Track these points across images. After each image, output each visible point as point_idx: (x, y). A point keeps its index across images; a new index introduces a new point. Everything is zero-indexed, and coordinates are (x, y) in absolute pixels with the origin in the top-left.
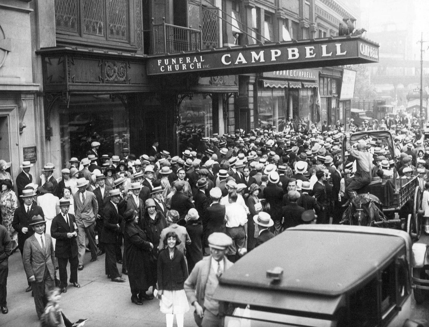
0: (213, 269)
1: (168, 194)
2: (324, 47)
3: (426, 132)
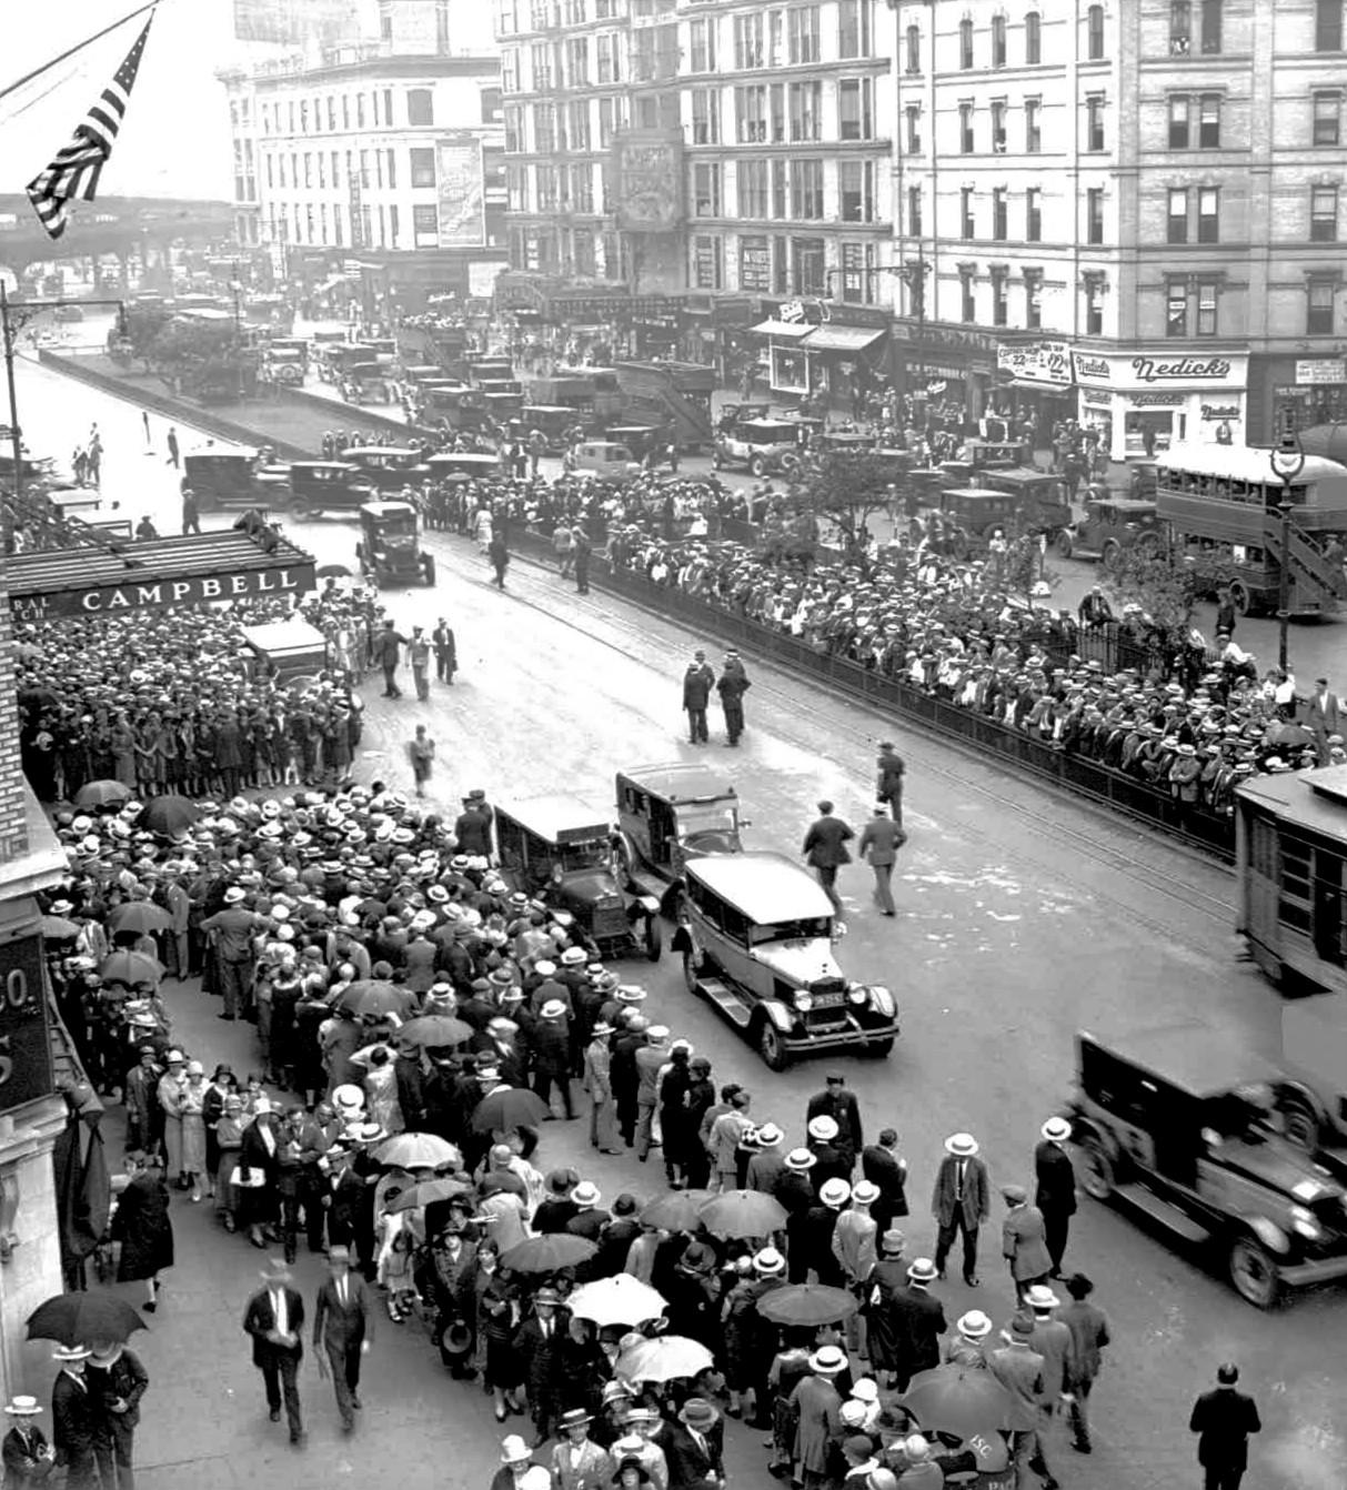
0: (748, 739)
1: (67, 702)
2: (262, 577)
3: (349, 522)
